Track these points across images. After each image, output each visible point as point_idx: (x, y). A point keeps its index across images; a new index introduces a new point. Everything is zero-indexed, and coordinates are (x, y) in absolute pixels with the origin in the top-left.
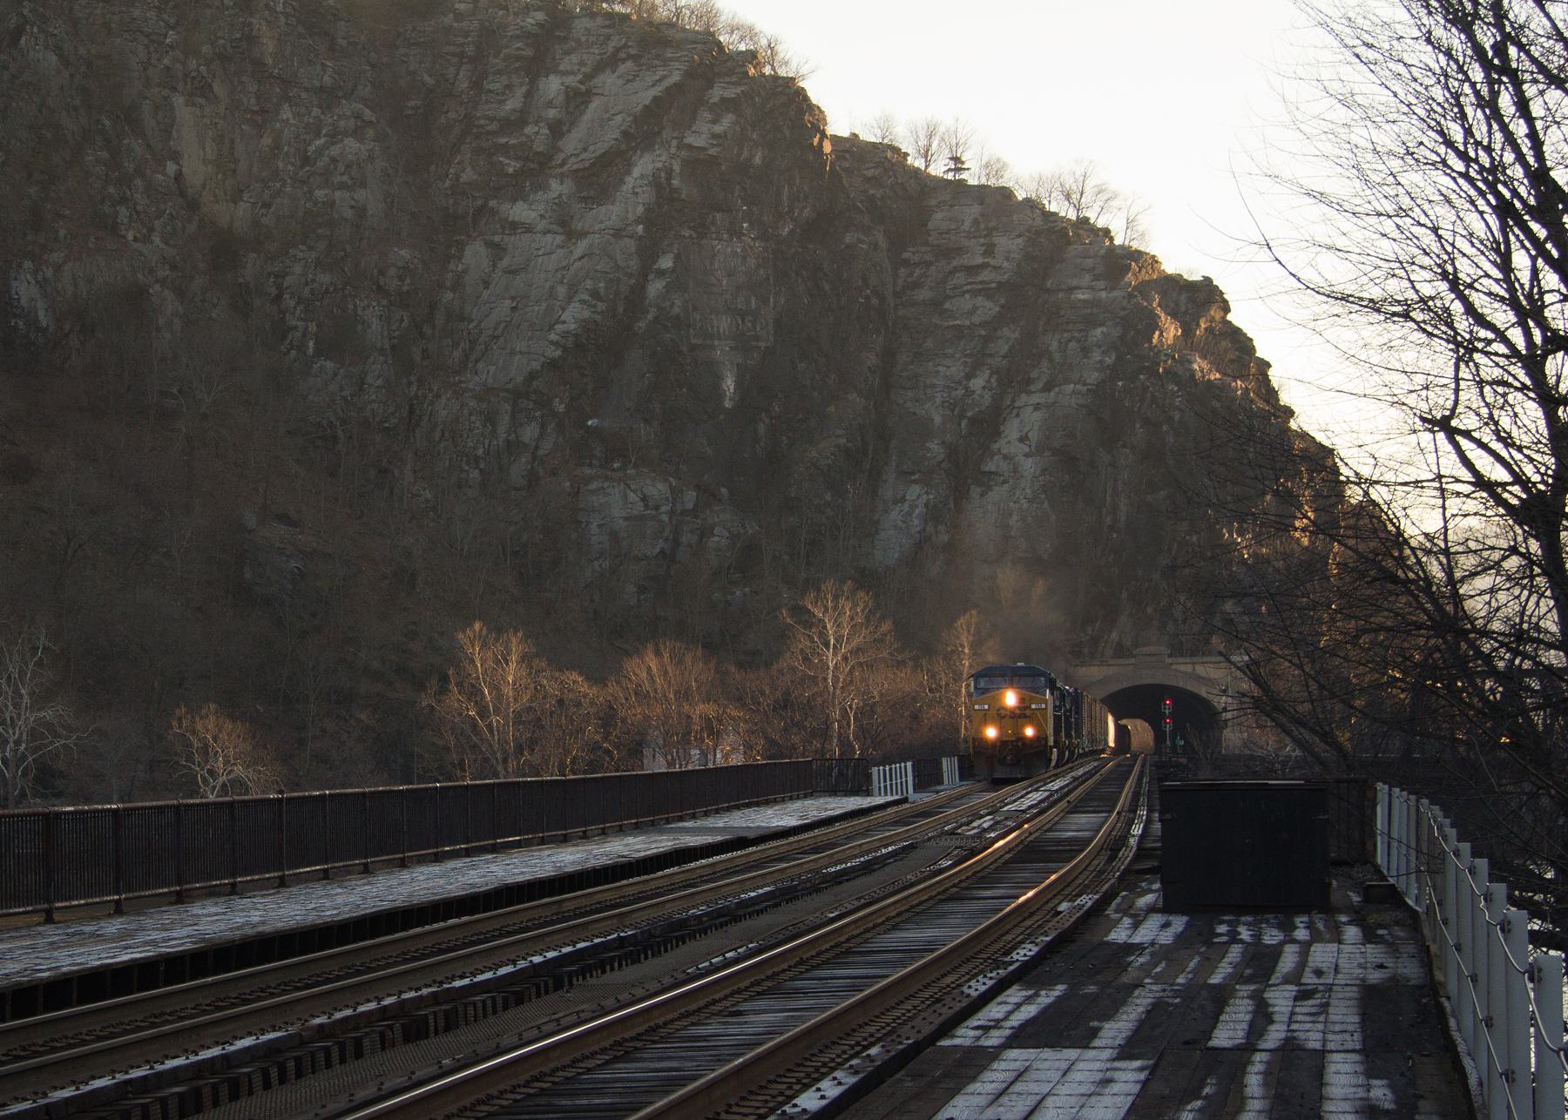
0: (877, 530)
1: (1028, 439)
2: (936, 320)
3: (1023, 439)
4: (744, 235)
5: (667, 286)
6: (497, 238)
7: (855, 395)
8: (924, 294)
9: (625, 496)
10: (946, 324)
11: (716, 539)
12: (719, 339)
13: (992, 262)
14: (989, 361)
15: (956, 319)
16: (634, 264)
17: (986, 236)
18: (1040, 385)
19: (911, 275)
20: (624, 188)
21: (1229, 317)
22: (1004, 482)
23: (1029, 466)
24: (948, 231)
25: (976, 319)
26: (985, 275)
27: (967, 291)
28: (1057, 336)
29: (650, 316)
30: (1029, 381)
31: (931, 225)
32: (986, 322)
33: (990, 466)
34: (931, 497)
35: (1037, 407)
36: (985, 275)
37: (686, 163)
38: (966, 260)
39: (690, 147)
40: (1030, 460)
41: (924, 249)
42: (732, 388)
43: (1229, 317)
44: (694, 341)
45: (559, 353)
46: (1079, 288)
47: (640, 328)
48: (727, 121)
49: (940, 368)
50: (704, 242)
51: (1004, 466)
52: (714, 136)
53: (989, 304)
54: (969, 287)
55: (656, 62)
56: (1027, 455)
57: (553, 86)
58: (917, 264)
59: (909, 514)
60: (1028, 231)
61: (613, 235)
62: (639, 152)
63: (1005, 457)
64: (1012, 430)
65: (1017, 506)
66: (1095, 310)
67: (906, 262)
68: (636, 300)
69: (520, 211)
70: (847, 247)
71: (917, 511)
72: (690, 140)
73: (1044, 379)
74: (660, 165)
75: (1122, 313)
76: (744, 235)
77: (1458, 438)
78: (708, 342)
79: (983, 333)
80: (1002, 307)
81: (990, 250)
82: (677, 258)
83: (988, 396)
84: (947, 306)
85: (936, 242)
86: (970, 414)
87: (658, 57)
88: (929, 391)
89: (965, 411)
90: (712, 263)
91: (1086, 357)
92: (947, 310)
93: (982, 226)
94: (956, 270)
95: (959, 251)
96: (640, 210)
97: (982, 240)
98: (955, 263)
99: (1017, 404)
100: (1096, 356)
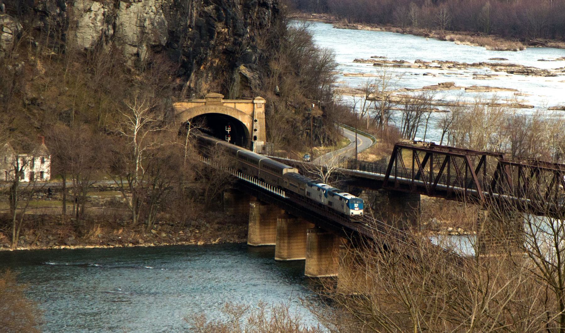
0: (77, 27)
11: (5, 34)
34: (106, 10)
59: (95, 19)
65: (148, 16)
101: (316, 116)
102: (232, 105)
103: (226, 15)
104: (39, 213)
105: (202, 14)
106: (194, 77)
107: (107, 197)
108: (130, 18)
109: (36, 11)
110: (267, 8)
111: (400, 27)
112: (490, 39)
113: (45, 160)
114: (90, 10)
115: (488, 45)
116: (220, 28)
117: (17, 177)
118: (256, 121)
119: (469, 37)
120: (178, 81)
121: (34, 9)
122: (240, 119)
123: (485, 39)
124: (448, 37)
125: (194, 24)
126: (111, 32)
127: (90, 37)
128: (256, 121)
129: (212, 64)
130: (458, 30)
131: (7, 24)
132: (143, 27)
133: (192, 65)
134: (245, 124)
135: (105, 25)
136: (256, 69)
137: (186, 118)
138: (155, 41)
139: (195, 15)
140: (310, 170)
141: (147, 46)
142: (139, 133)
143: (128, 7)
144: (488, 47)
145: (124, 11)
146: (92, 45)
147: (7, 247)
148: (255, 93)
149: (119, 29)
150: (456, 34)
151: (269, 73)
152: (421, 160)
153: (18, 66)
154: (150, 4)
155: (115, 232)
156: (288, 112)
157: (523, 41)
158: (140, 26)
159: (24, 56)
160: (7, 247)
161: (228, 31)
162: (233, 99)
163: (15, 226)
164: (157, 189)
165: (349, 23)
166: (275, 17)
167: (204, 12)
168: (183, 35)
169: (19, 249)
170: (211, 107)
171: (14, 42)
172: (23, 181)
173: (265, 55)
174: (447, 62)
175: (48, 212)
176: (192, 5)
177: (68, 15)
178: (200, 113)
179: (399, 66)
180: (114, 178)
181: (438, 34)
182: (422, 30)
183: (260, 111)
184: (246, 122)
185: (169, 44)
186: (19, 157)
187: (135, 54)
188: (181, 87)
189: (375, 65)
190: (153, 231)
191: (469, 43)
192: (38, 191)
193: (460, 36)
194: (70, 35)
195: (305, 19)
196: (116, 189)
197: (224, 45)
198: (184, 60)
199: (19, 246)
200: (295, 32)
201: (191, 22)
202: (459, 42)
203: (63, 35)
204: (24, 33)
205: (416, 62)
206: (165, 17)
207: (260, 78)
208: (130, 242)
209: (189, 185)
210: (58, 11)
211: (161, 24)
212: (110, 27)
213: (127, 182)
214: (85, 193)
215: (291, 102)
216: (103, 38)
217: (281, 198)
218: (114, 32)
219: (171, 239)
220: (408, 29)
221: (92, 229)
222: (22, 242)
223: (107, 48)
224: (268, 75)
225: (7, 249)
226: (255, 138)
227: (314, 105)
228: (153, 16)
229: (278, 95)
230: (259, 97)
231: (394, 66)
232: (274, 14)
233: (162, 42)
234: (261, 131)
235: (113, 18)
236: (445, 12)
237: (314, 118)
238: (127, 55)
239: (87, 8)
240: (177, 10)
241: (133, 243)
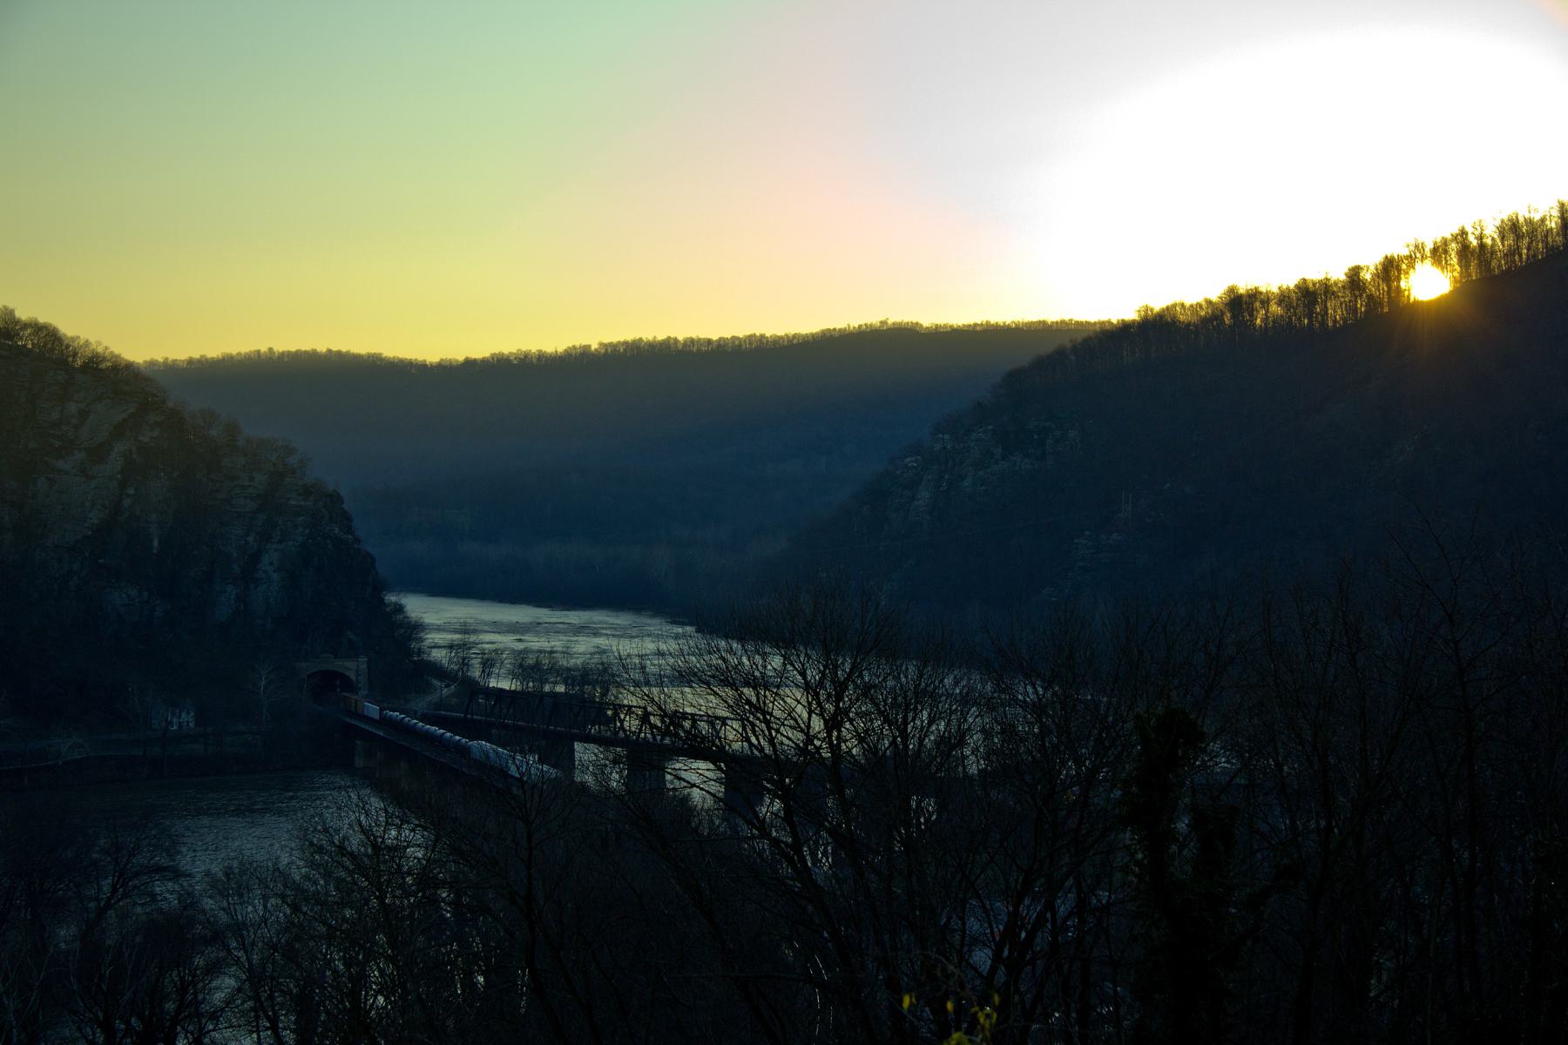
3: (271, 564)
6: (52, 476)
13: (252, 484)
21: (344, 506)
23: (276, 577)
35: (276, 550)
43: (344, 506)
45: (90, 533)
48: (156, 433)
56: (274, 572)
57: (72, 408)
69: (61, 464)
71: (232, 597)
81: (252, 479)
84: (233, 502)
86: (249, 553)
100: (301, 529)
102: (341, 663)
122: (347, 674)
126: (242, 608)
152: (791, 668)
183: (364, 667)
184: (353, 677)
200: (391, 603)
217: (380, 735)
226: (360, 688)
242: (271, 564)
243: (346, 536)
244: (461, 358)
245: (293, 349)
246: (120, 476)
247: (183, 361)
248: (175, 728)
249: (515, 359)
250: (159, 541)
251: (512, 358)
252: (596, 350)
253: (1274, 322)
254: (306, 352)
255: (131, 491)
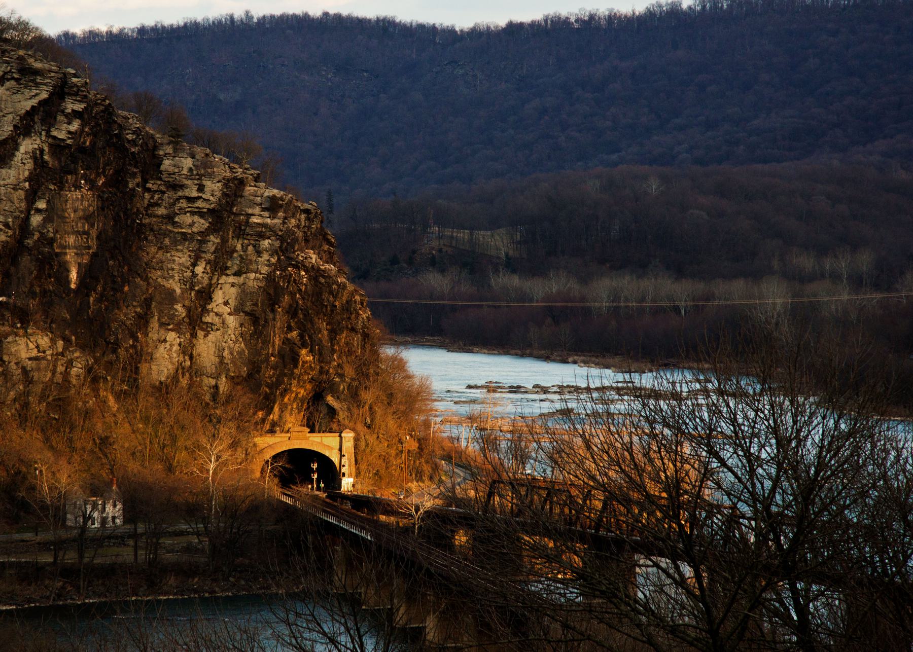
0: (151, 359)
1: (229, 304)
2: (170, 227)
3: (226, 303)
4: (82, 187)
5: (44, 219)
7: (139, 279)
8: (161, 211)
9: (27, 345)
10: (176, 230)
11: (75, 369)
12: (69, 249)
13: (204, 196)
14: (203, 255)
15: (182, 228)
16: (23, 205)
17: (198, 179)
18: (233, 271)
19: (152, 197)
20: (15, 159)
22: (217, 330)
23: (232, 321)
24: (174, 174)
25: (195, 230)
26: (199, 204)
27: (188, 212)
28: (240, 242)
29: (36, 238)
30: (227, 268)
31: (162, 168)
32: (201, 232)
33: (208, 319)
34: (182, 340)
35: (233, 285)
36: (199, 204)
37: (51, 146)
38: (187, 193)
39: (55, 138)
40: (232, 317)
41: (159, 182)
42: (75, 277)
44: (56, 251)
46: (254, 215)
47: (28, 243)
48: (75, 126)
49: (176, 259)
50: (62, 192)
51: (216, 320)
52: (69, 132)
53: (202, 221)
54: (189, 209)
55: (31, 84)
56: (230, 314)
58: (156, 191)
59: (170, 350)
60: (224, 179)
61: (13, 189)
62: (22, 137)
63: (217, 314)
64: (218, 297)
65: (227, 345)
66: (263, 229)
67: (149, 190)
68: (24, 227)
70: (130, 190)
72: (54, 133)
73: (236, 268)
74: (36, 146)
75: (280, 233)
76: (82, 187)
77: (652, 564)
78: (64, 251)
79: (199, 238)
80: (210, 223)
81: (201, 188)
82: (48, 202)
83: (206, 277)
84: (176, 219)
85: (167, 180)
86: (196, 288)
87: (32, 81)
88: (170, 272)
89: (194, 286)
90: (66, 205)
91: (259, 256)
92: (177, 222)
93: (195, 172)
94: (181, 198)
95: (182, 187)
96: (27, 173)
97: (196, 182)
98: (180, 193)
99: (220, 282)
100: (266, 256)
101: (411, 449)
102: (318, 440)
103: (311, 341)
104: (108, 561)
105: (286, 341)
106: (277, 409)
107: (182, 541)
108: (208, 347)
109: (108, 343)
110: (357, 332)
111: (520, 349)
112: (617, 359)
113: (117, 503)
114: (165, 341)
115: (613, 366)
116: (305, 355)
117: (85, 523)
118: (344, 456)
119: (593, 359)
120: (260, 414)
121: (105, 341)
122: (327, 454)
123: (611, 361)
124: (570, 359)
125: (276, 352)
126: (188, 363)
127: (165, 370)
128: (344, 456)
129: (297, 395)
130: (582, 352)
131: (77, 358)
132: (222, 358)
133: (275, 396)
134: (333, 459)
135: (181, 356)
136: (345, 400)
137: (268, 455)
138: (234, 372)
139: (277, 343)
140: (401, 509)
141: (226, 377)
142: (215, 473)
143: (206, 336)
144: (614, 369)
145: (201, 341)
146: (168, 378)
147: (74, 599)
148: (344, 425)
149: (196, 360)
150: (580, 356)
151: (359, 404)
153: (88, 402)
154: (229, 333)
155: (190, 580)
156: (381, 445)
157: (652, 361)
158: (219, 356)
159: (96, 391)
160: (74, 599)
161: (314, 359)
162: (319, 432)
163: (82, 577)
164: (235, 533)
165: (465, 345)
166: (365, 343)
167: (287, 339)
168: (265, 365)
169: (87, 601)
170: (295, 441)
171: (85, 377)
172: (93, 526)
173: (355, 384)
174: (568, 386)
175: (120, 560)
176: (274, 332)
177: (141, 346)
178: (285, 449)
179: (515, 392)
180: (187, 522)
181: (560, 356)
182: (543, 352)
183: (349, 444)
185: (250, 375)
186: (89, 501)
187: (213, 387)
188: (263, 421)
189: (489, 391)
190: (231, 579)
191: (593, 365)
192: (109, 537)
193: (584, 358)
194: (144, 368)
195: (396, 344)
196: (193, 534)
197: (309, 374)
198: (266, 392)
199: (86, 598)
200: (388, 359)
201: (274, 349)
202: (582, 365)
203: (137, 368)
204: (96, 367)
205: (533, 387)
206: (246, 345)
207: (349, 409)
208: (206, 592)
209: (270, 528)
210: (131, 342)
211: (241, 353)
212: (187, 358)
213: (202, 526)
214: (158, 539)
215: (383, 435)
216: (180, 368)
218: (191, 364)
219: (251, 587)
220: (528, 352)
221: (166, 578)
222: (91, 593)
223: (184, 382)
224: (358, 406)
225: (74, 602)
226: (344, 475)
227: (408, 438)
228: (232, 345)
229: (369, 427)
230: (348, 430)
231: (510, 392)
232: (365, 339)
233: (242, 373)
234: (350, 466)
235: (189, 348)
236: (567, 332)
237: (409, 451)
238: (205, 388)
239: (162, 339)
240: (258, 338)
241: (209, 593)
242: (226, 303)
243: (327, 266)
244: (502, 23)
245: (277, 12)
246: (27, 184)
247: (133, 30)
248: (96, 525)
249: (577, 21)
250: (77, 273)
251: (573, 20)
252: (690, 8)
253: (552, 21)
254: (295, 17)
255: (42, 205)
